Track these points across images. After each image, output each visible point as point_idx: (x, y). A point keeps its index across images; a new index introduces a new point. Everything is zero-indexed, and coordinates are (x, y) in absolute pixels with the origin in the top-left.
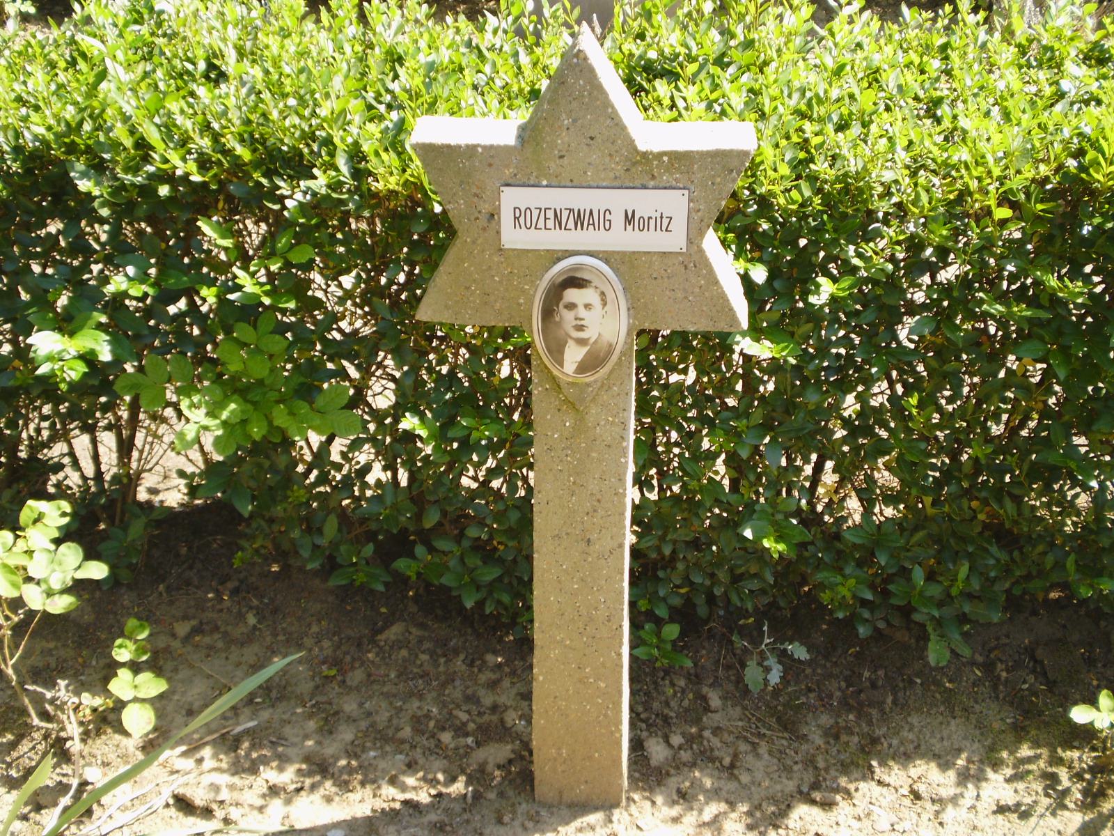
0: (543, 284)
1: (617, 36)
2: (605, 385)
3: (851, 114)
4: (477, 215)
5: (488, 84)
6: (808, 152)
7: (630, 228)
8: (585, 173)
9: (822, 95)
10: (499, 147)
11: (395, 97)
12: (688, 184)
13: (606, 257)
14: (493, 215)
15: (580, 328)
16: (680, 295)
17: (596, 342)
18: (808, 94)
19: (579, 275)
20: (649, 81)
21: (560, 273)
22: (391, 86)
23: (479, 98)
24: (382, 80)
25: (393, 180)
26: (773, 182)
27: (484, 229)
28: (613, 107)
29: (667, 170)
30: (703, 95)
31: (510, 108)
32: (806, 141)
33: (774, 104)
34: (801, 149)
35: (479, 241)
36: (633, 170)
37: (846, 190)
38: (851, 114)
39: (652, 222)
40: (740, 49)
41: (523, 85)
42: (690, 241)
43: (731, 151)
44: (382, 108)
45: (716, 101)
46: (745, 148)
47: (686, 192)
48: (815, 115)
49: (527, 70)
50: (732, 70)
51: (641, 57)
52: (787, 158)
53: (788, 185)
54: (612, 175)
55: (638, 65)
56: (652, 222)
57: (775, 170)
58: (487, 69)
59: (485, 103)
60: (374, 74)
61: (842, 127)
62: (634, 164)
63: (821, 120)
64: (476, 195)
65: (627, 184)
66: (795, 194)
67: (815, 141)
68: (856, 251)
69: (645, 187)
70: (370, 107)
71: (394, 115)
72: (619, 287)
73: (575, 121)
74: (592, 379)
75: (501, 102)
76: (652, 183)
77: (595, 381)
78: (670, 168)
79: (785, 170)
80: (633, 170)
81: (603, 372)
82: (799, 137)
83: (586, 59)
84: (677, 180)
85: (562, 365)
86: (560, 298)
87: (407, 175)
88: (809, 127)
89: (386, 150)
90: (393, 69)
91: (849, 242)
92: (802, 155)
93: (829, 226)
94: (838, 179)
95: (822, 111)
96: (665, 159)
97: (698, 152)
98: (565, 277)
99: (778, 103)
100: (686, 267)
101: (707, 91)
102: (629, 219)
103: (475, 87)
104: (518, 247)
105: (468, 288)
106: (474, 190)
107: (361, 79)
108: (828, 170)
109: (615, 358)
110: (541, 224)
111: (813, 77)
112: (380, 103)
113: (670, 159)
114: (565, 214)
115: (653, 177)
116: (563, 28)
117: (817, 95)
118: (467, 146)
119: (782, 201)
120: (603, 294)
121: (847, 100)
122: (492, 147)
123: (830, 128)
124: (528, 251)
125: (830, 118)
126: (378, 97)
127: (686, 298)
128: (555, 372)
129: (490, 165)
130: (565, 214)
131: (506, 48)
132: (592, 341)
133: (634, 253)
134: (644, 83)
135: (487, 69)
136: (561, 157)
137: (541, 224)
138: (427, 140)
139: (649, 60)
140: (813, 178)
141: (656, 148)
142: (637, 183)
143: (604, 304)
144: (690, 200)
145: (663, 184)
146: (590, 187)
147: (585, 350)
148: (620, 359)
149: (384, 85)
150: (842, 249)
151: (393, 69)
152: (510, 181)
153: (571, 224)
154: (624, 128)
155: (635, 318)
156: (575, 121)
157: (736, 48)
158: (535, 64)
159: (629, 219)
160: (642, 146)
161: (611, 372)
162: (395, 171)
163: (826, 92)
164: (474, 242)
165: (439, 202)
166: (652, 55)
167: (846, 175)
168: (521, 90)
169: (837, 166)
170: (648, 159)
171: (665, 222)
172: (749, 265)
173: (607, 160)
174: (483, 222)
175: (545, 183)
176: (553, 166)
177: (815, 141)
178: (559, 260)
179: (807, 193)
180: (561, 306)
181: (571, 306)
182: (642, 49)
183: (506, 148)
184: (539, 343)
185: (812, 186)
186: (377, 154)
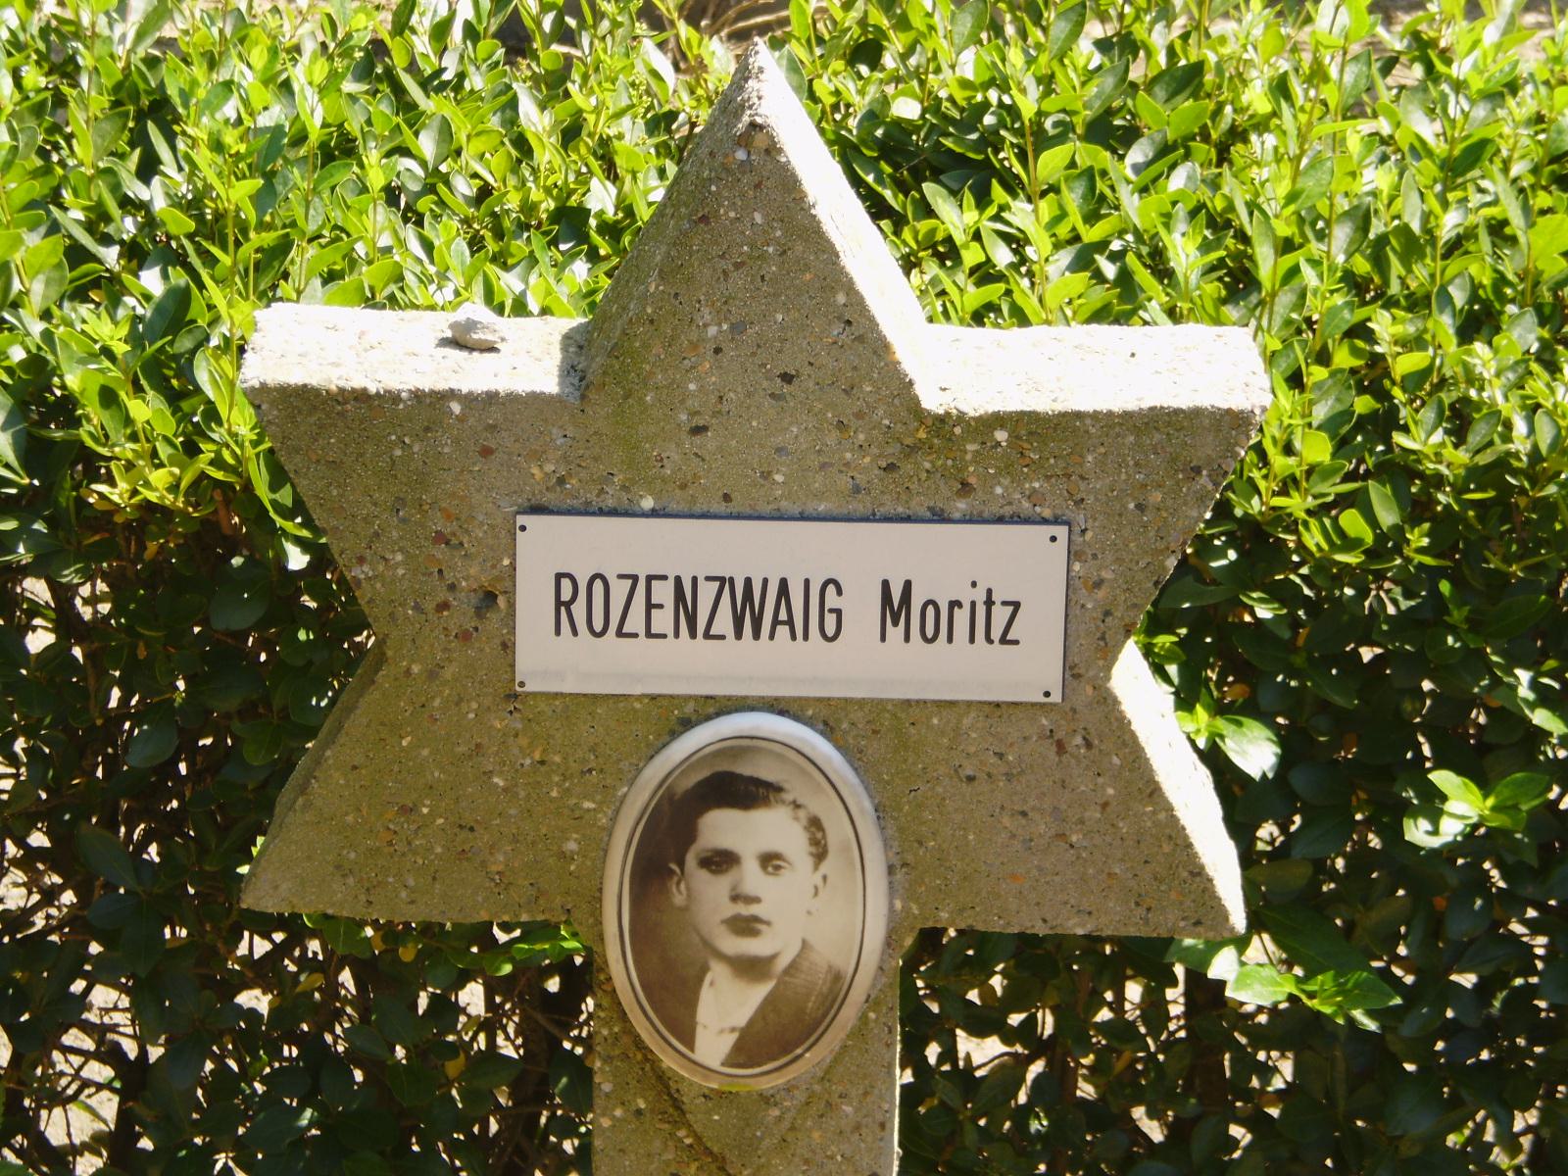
0: (640, 797)
1: (801, 53)
2: (820, 1102)
3: (1501, 280)
4: (443, 595)
5: (430, 189)
6: (1383, 396)
7: (895, 633)
8: (766, 475)
9: (1416, 226)
10: (513, 398)
11: (150, 223)
12: (1070, 511)
13: (825, 715)
14: (490, 597)
15: (747, 926)
16: (1042, 827)
17: (793, 968)
18: (1377, 228)
19: (746, 769)
20: (902, 187)
21: (689, 763)
22: (136, 189)
23: (409, 233)
24: (109, 171)
25: (160, 478)
26: (1284, 490)
27: (465, 636)
28: (849, 287)
29: (1007, 469)
30: (1063, 231)
31: (501, 260)
32: (1376, 361)
33: (1288, 260)
34: (1362, 390)
35: (448, 673)
36: (907, 468)
37: (1502, 507)
38: (1501, 280)
39: (962, 617)
40: (1160, 92)
41: (536, 195)
42: (1072, 672)
43: (1196, 413)
44: (111, 255)
45: (1102, 246)
46: (1237, 402)
47: (1061, 532)
48: (1395, 288)
49: (546, 154)
50: (1138, 154)
51: (872, 117)
52: (1320, 413)
53: (1332, 489)
54: (844, 482)
55: (867, 138)
56: (962, 617)
57: (1288, 450)
58: (426, 144)
59: (428, 246)
60: (84, 153)
61: (1478, 323)
62: (912, 450)
63: (1417, 303)
64: (440, 538)
65: (889, 508)
66: (1352, 521)
67: (1405, 364)
68: (1534, 685)
69: (940, 517)
70: (76, 254)
71: (151, 280)
72: (862, 804)
73: (738, 328)
74: (779, 1080)
75: (476, 244)
76: (962, 505)
77: (789, 1088)
78: (1014, 463)
79: (1318, 449)
80: (907, 468)
81: (814, 1058)
82: (1355, 352)
83: (772, 149)
84: (1033, 496)
85: (688, 1037)
86: (690, 835)
87: (202, 462)
88: (1385, 325)
89: (138, 389)
90: (140, 139)
91: (1514, 661)
92: (1363, 404)
93: (1457, 615)
94: (1478, 475)
95: (1420, 275)
96: (1001, 436)
97: (1095, 416)
98: (704, 773)
99: (1298, 257)
100: (1061, 747)
101: (1075, 218)
102: (895, 606)
103: (391, 195)
104: (569, 686)
105: (407, 810)
106: (439, 524)
107: (47, 170)
108: (1449, 452)
109: (849, 1014)
110: (635, 622)
111: (1378, 178)
112: (106, 240)
113: (1015, 437)
114: (707, 592)
115: (965, 488)
116: (641, 28)
117: (1405, 230)
118: (418, 395)
119: (1314, 539)
120: (815, 824)
121: (1485, 241)
122: (492, 397)
123: (1444, 325)
124: (595, 698)
125: (1446, 299)
126: (97, 221)
127: (1061, 836)
128: (669, 1061)
129: (486, 452)
130: (707, 592)
131: (476, 81)
132: (782, 963)
133: (908, 702)
134: (888, 194)
135: (426, 144)
136: (698, 430)
137: (635, 622)
138: (295, 377)
139: (898, 123)
140: (1400, 471)
141: (976, 403)
142: (919, 506)
143: (820, 854)
144: (1073, 554)
145: (997, 509)
146: (780, 516)
147: (759, 992)
148: (863, 1018)
149: (116, 188)
150: (1497, 682)
151: (140, 139)
152: (548, 499)
153: (724, 623)
154: (882, 347)
155: (910, 895)
156: (738, 328)
157: (1151, 84)
158: (570, 134)
159: (895, 606)
160: (932, 401)
161: (837, 1059)
162: (164, 451)
163: (1426, 217)
164: (432, 675)
165: (299, 541)
166: (907, 109)
167: (1502, 464)
168: (527, 208)
169: (1474, 439)
170: (950, 439)
171: (1001, 615)
172: (1221, 724)
173: (832, 438)
174: (461, 615)
175: (648, 503)
176: (675, 455)
177: (1405, 364)
178: (687, 724)
179: (1388, 517)
180: (691, 860)
181: (721, 861)
182: (872, 91)
183: (536, 399)
184: (620, 968)
185: (1401, 497)
186: (108, 397)
